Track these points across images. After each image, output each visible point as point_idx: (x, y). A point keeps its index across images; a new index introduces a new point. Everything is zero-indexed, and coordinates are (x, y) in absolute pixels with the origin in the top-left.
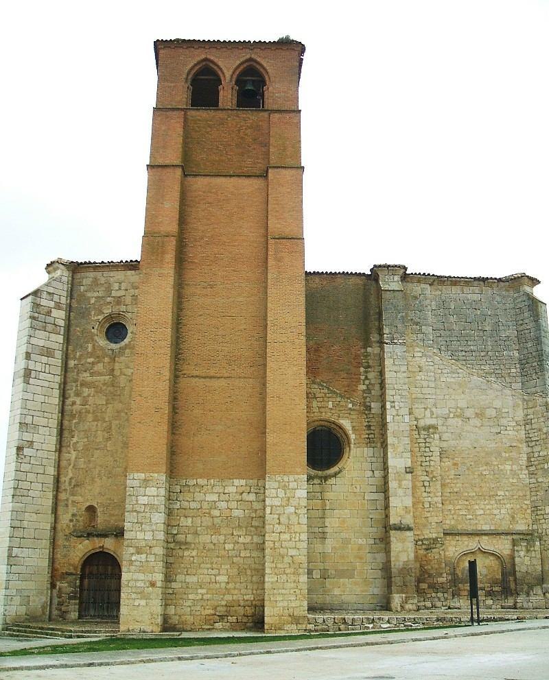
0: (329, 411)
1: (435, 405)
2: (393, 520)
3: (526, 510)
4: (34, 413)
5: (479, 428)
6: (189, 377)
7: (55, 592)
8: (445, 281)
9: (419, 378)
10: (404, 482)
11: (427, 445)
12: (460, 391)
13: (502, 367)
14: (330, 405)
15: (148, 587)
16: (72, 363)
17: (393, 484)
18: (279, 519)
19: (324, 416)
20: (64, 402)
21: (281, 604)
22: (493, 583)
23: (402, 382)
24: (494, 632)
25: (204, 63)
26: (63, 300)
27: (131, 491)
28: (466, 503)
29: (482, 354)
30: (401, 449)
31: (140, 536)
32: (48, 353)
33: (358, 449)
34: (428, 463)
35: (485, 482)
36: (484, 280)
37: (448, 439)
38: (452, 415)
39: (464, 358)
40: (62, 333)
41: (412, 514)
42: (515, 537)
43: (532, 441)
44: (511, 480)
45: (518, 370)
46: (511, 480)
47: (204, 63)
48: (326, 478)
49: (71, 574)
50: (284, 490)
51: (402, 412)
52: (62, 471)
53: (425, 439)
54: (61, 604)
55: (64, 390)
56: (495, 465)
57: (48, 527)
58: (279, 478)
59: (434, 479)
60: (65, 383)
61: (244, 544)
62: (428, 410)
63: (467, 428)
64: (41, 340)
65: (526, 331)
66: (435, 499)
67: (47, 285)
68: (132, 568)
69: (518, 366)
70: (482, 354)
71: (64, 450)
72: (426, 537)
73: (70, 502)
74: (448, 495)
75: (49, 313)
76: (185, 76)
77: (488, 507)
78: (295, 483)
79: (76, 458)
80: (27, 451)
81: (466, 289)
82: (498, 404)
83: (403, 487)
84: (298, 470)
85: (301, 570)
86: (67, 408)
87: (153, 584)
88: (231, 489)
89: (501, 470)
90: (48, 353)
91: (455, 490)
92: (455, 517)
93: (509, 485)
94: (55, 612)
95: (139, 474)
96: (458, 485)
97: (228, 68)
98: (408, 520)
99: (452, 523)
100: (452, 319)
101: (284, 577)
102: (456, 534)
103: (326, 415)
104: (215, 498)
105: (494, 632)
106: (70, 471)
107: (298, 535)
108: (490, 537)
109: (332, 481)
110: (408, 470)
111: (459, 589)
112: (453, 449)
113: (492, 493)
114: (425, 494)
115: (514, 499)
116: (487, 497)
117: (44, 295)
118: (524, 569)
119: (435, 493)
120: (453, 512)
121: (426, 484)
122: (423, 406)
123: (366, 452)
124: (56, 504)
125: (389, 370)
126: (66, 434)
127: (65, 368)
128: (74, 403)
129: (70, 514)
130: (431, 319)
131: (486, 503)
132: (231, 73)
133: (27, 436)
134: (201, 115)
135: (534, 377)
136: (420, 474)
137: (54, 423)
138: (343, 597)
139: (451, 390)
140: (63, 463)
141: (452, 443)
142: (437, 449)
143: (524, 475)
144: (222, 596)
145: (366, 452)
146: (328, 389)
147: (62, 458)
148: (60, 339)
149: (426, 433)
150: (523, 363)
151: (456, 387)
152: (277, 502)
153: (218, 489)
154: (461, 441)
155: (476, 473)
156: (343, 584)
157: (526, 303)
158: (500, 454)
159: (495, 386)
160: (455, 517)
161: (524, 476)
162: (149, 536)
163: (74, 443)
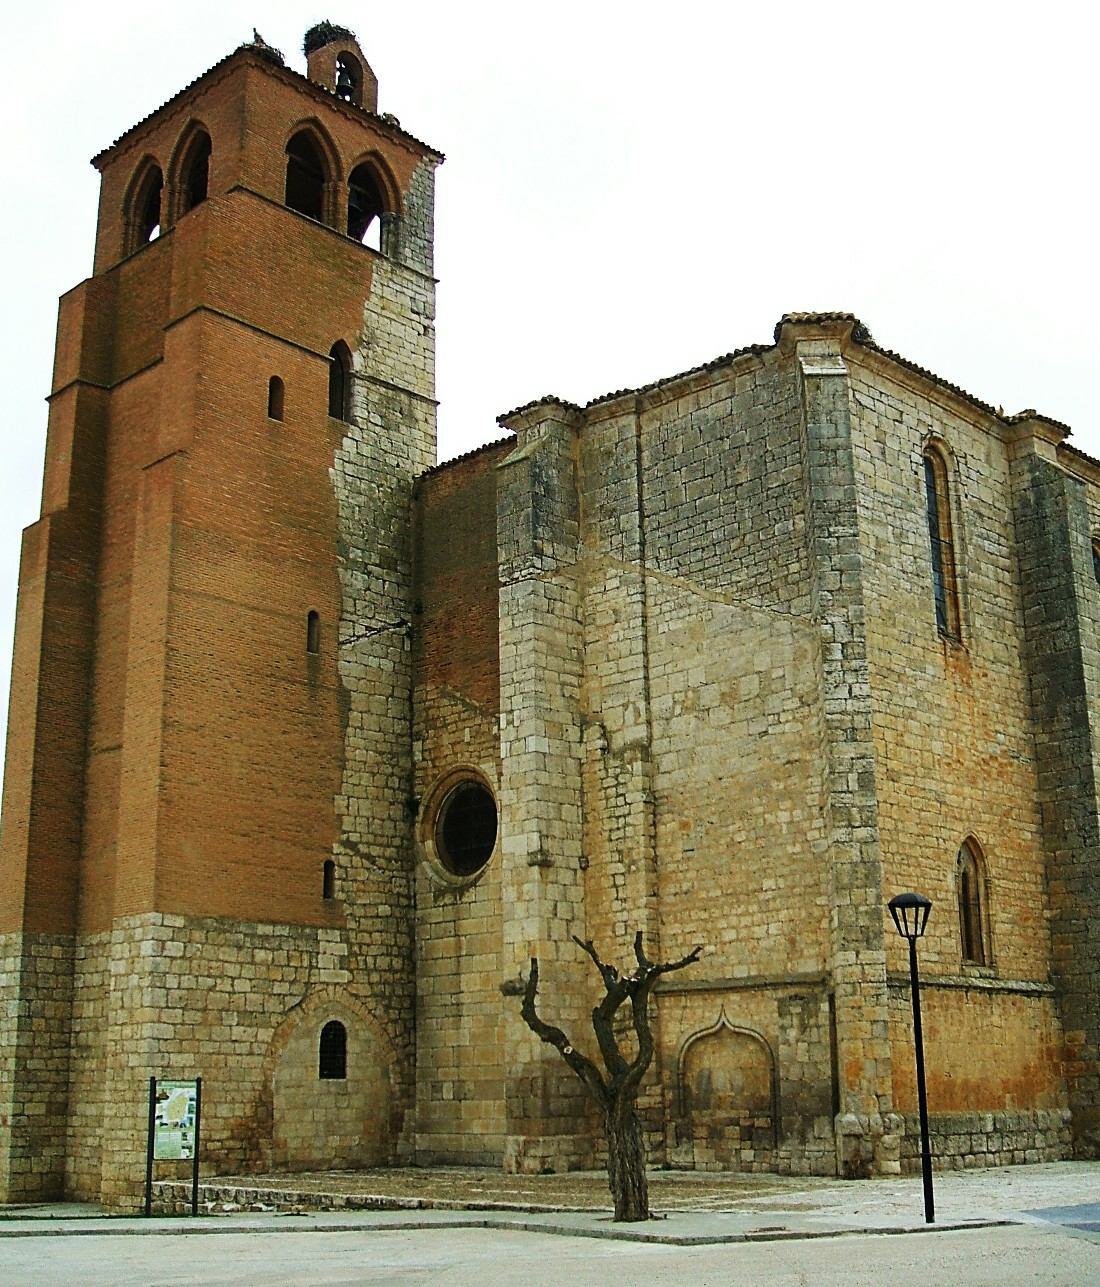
0: (465, 747)
3: (819, 921)
8: (658, 395)
10: (526, 887)
11: (621, 790)
13: (772, 565)
22: (756, 1108)
24: (345, 1229)
28: (704, 915)
34: (620, 834)
36: (724, 362)
38: (678, 710)
39: (700, 566)
46: (790, 849)
53: (616, 778)
59: (633, 868)
62: (631, 707)
63: (707, 733)
70: (734, 545)
81: (704, 397)
82: (762, 662)
85: (140, 1095)
89: (772, 826)
93: (785, 861)
96: (688, 875)
100: (679, 478)
105: (345, 1229)
108: (746, 994)
111: (693, 1123)
112: (681, 789)
114: (617, 905)
115: (794, 895)
116: (742, 897)
118: (794, 1073)
119: (634, 900)
120: (680, 939)
121: (620, 880)
131: (739, 911)
136: (608, 859)
138: (486, 1138)
146: (464, 703)
149: (618, 763)
151: (684, 639)
154: (695, 769)
158: (768, 789)
159: (756, 616)
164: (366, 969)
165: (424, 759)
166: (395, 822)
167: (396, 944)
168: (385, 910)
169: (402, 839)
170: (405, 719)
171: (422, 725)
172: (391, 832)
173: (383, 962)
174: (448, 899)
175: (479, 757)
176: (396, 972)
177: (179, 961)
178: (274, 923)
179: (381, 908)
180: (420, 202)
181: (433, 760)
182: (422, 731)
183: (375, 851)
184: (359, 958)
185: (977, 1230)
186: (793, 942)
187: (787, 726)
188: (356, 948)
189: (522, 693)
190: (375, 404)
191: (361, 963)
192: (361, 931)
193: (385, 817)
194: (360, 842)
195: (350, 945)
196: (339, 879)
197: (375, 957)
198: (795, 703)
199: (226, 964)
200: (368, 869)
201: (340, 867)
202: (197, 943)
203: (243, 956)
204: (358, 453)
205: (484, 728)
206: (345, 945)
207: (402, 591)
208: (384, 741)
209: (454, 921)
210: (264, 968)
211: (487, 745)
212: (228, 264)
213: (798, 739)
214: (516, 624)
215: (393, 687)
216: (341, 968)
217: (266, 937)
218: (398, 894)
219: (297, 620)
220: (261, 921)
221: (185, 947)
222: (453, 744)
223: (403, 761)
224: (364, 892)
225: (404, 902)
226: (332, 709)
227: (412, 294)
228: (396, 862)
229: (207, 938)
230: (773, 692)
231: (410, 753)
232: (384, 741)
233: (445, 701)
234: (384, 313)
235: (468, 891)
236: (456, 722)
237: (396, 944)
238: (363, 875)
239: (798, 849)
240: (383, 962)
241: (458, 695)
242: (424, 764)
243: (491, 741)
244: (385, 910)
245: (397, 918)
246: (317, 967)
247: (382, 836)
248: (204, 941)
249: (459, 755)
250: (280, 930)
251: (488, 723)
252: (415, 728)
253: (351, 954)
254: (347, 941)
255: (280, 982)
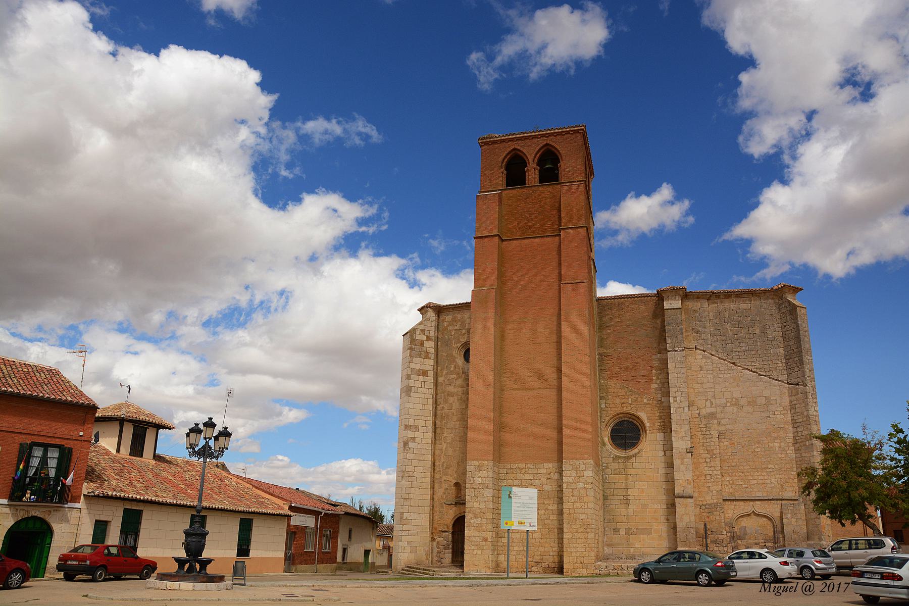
1: (714, 397)
2: (678, 490)
4: (415, 417)
5: (752, 414)
6: (510, 390)
7: (435, 543)
9: (700, 376)
12: (736, 384)
13: (770, 362)
14: (630, 401)
15: (482, 541)
16: (440, 379)
17: (676, 462)
18: (572, 492)
19: (625, 410)
20: (436, 408)
21: (575, 554)
23: (682, 381)
25: (513, 152)
26: (433, 334)
27: (469, 474)
29: (753, 353)
30: (682, 434)
31: (476, 505)
32: (424, 373)
33: (652, 434)
34: (708, 444)
35: (758, 457)
37: (725, 424)
38: (728, 404)
40: (433, 358)
41: (692, 485)
42: (784, 502)
43: (796, 423)
44: (780, 456)
45: (784, 364)
46: (780, 456)
47: (513, 152)
48: (628, 458)
49: (445, 532)
50: (576, 471)
51: (683, 405)
52: (437, 457)
54: (439, 552)
55: (436, 399)
56: (765, 444)
57: (429, 497)
58: (572, 463)
60: (436, 394)
61: (552, 510)
62: (709, 401)
64: (417, 364)
65: (789, 332)
66: (715, 472)
67: (421, 323)
68: (472, 528)
69: (783, 361)
70: (753, 353)
71: (438, 442)
72: (708, 502)
73: (443, 480)
74: (727, 468)
75: (422, 344)
76: (500, 164)
77: (760, 478)
78: (584, 466)
79: (446, 448)
80: (411, 445)
82: (766, 393)
83: (684, 464)
84: (586, 456)
86: (438, 412)
87: (485, 540)
88: (543, 471)
89: (771, 447)
90: (424, 373)
91: (733, 464)
92: (733, 486)
94: (435, 558)
95: (475, 462)
96: (735, 460)
97: (531, 153)
98: (689, 490)
99: (730, 491)
100: (728, 326)
101: (577, 535)
102: (733, 500)
103: (620, 410)
104: (531, 477)
106: (442, 458)
107: (586, 504)
109: (633, 460)
110: (688, 451)
112: (730, 431)
113: (763, 467)
114: (706, 469)
117: (418, 332)
120: (731, 482)
121: (708, 460)
122: (704, 398)
123: (658, 437)
124: (433, 481)
125: (671, 372)
126: (438, 431)
127: (436, 384)
128: (443, 408)
129: (443, 488)
130: (709, 327)
132: (533, 157)
133: (410, 434)
134: (517, 192)
135: (796, 370)
137: (430, 424)
139: (727, 384)
140: (437, 452)
141: (729, 426)
142: (716, 432)
143: (791, 452)
144: (537, 548)
145: (658, 437)
147: (437, 448)
148: (431, 362)
150: (788, 358)
152: (571, 480)
153: (532, 471)
155: (750, 451)
156: (643, 540)
157: (788, 309)
160: (733, 486)
161: (791, 452)
162: (482, 506)
163: (444, 437)
185: (545, 585)
186: (782, 486)
187: (778, 416)
198: (781, 409)
213: (783, 421)
214: (677, 366)
230: (771, 404)
239: (783, 456)
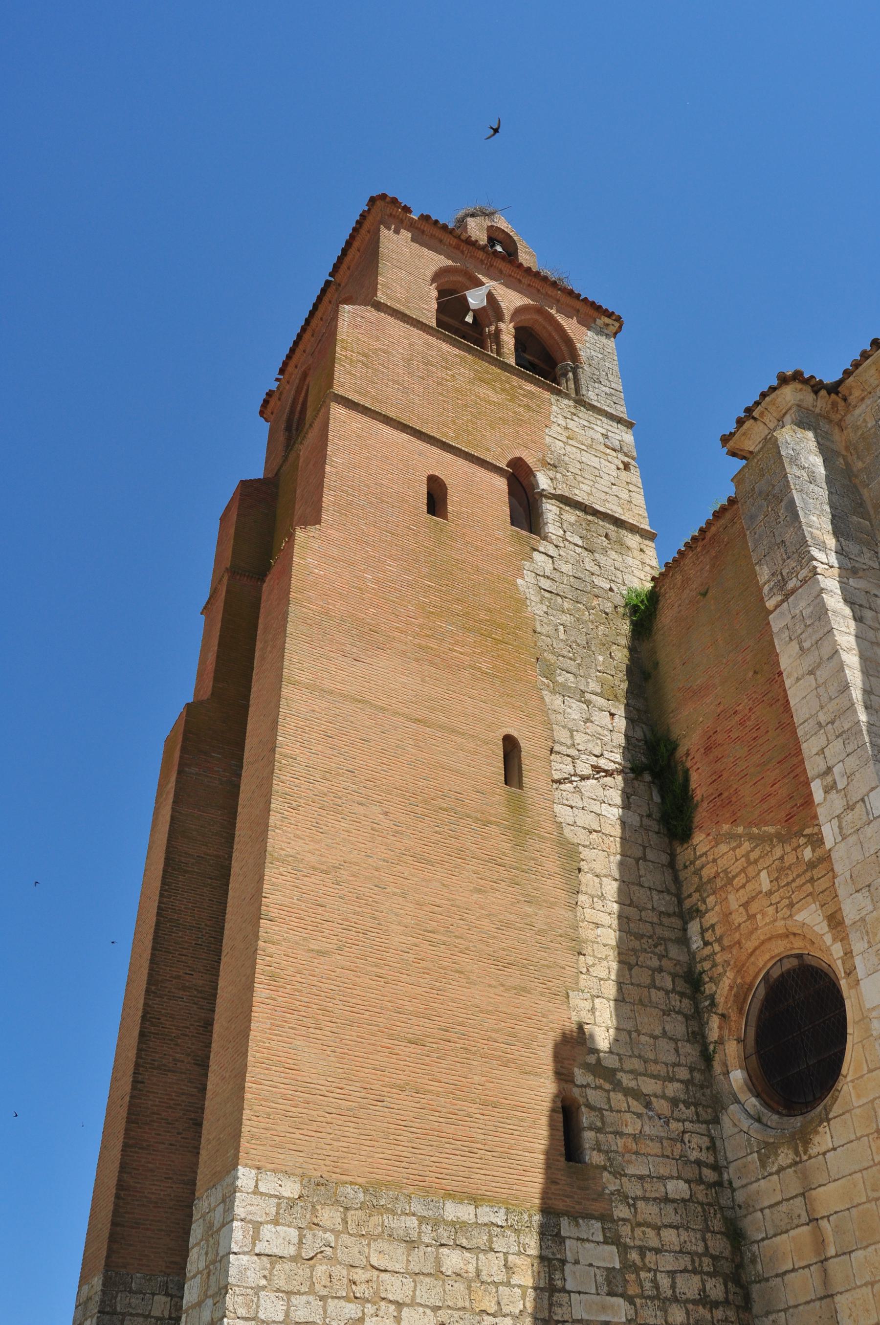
146: (751, 838)
164: (657, 1297)
165: (706, 944)
166: (676, 1041)
167: (707, 1252)
168: (677, 1188)
169: (692, 1070)
170: (669, 892)
171: (696, 896)
172: (672, 1058)
173: (689, 1286)
174: (785, 1157)
175: (791, 905)
176: (715, 1305)
177: (287, 1266)
178: (475, 1200)
179: (671, 1185)
180: (600, 356)
181: (719, 940)
182: (697, 904)
183: (649, 1086)
184: (643, 1275)
188: (634, 1256)
189: (840, 735)
190: (572, 524)
191: (648, 1285)
192: (639, 1225)
193: (658, 1032)
194: (622, 1070)
195: (623, 1249)
196: (590, 1129)
197: (672, 1274)
199: (384, 1276)
200: (639, 1116)
201: (589, 1106)
202: (325, 1231)
203: (419, 1260)
204: (555, 569)
205: (790, 859)
206: (614, 1248)
207: (637, 728)
208: (640, 920)
209: (803, 1194)
210: (460, 1287)
211: (799, 882)
212: (363, 364)
214: (806, 645)
215: (645, 848)
216: (611, 1294)
217: (459, 1226)
218: (699, 1163)
219: (486, 743)
220: (450, 1195)
221: (301, 1238)
222: (745, 905)
223: (674, 951)
224: (636, 1153)
225: (709, 1175)
226: (552, 864)
227: (604, 431)
228: (687, 1108)
229: (345, 1221)
231: (684, 941)
232: (640, 920)
233: (723, 848)
234: (570, 442)
235: (817, 1133)
236: (743, 870)
237: (707, 1252)
238: (632, 1126)
240: (689, 1286)
241: (740, 830)
242: (707, 951)
243: (806, 871)
244: (677, 1188)
245: (702, 1204)
246: (563, 1290)
247: (656, 1062)
248: (340, 1228)
249: (759, 917)
250: (486, 1214)
251: (795, 849)
252: (687, 904)
253: (628, 1266)
254: (612, 1239)
255: (494, 1315)
